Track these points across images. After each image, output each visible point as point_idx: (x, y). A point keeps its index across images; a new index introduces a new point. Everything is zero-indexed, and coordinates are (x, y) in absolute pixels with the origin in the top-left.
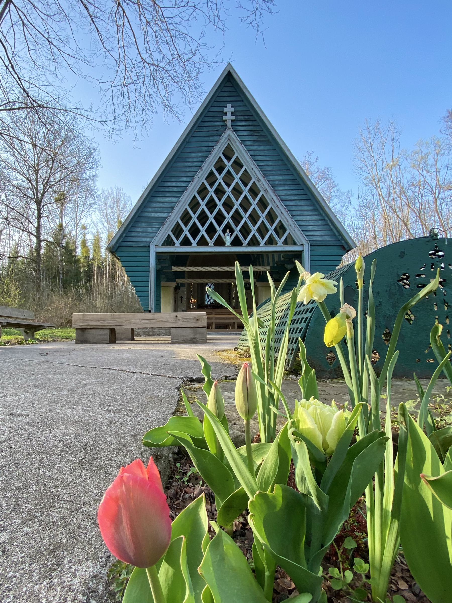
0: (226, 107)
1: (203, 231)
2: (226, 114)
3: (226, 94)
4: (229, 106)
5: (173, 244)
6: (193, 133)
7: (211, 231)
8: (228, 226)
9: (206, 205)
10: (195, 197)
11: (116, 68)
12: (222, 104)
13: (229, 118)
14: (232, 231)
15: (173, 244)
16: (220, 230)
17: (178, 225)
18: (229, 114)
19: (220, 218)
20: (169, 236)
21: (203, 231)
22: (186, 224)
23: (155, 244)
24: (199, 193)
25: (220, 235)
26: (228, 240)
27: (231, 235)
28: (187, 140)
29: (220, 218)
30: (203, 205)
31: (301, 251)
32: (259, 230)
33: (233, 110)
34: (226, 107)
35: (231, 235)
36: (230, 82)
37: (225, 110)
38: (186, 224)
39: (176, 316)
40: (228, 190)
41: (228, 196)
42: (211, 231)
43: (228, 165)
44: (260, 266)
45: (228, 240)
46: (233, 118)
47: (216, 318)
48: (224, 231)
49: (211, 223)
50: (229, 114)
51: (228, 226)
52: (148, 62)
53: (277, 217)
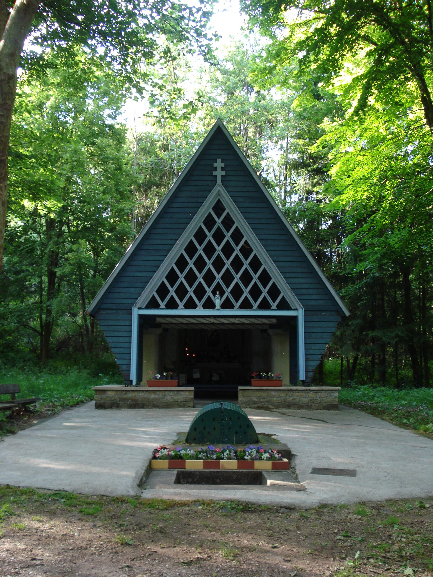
4: (219, 160)
7: (200, 291)
13: (219, 173)
16: (209, 291)
17: (210, 215)
18: (219, 169)
19: (209, 278)
20: (191, 241)
26: (218, 302)
29: (209, 278)
33: (223, 165)
35: (221, 298)
37: (215, 165)
42: (200, 291)
45: (218, 302)
46: (224, 173)
48: (214, 293)
50: (219, 169)
53: (270, 279)
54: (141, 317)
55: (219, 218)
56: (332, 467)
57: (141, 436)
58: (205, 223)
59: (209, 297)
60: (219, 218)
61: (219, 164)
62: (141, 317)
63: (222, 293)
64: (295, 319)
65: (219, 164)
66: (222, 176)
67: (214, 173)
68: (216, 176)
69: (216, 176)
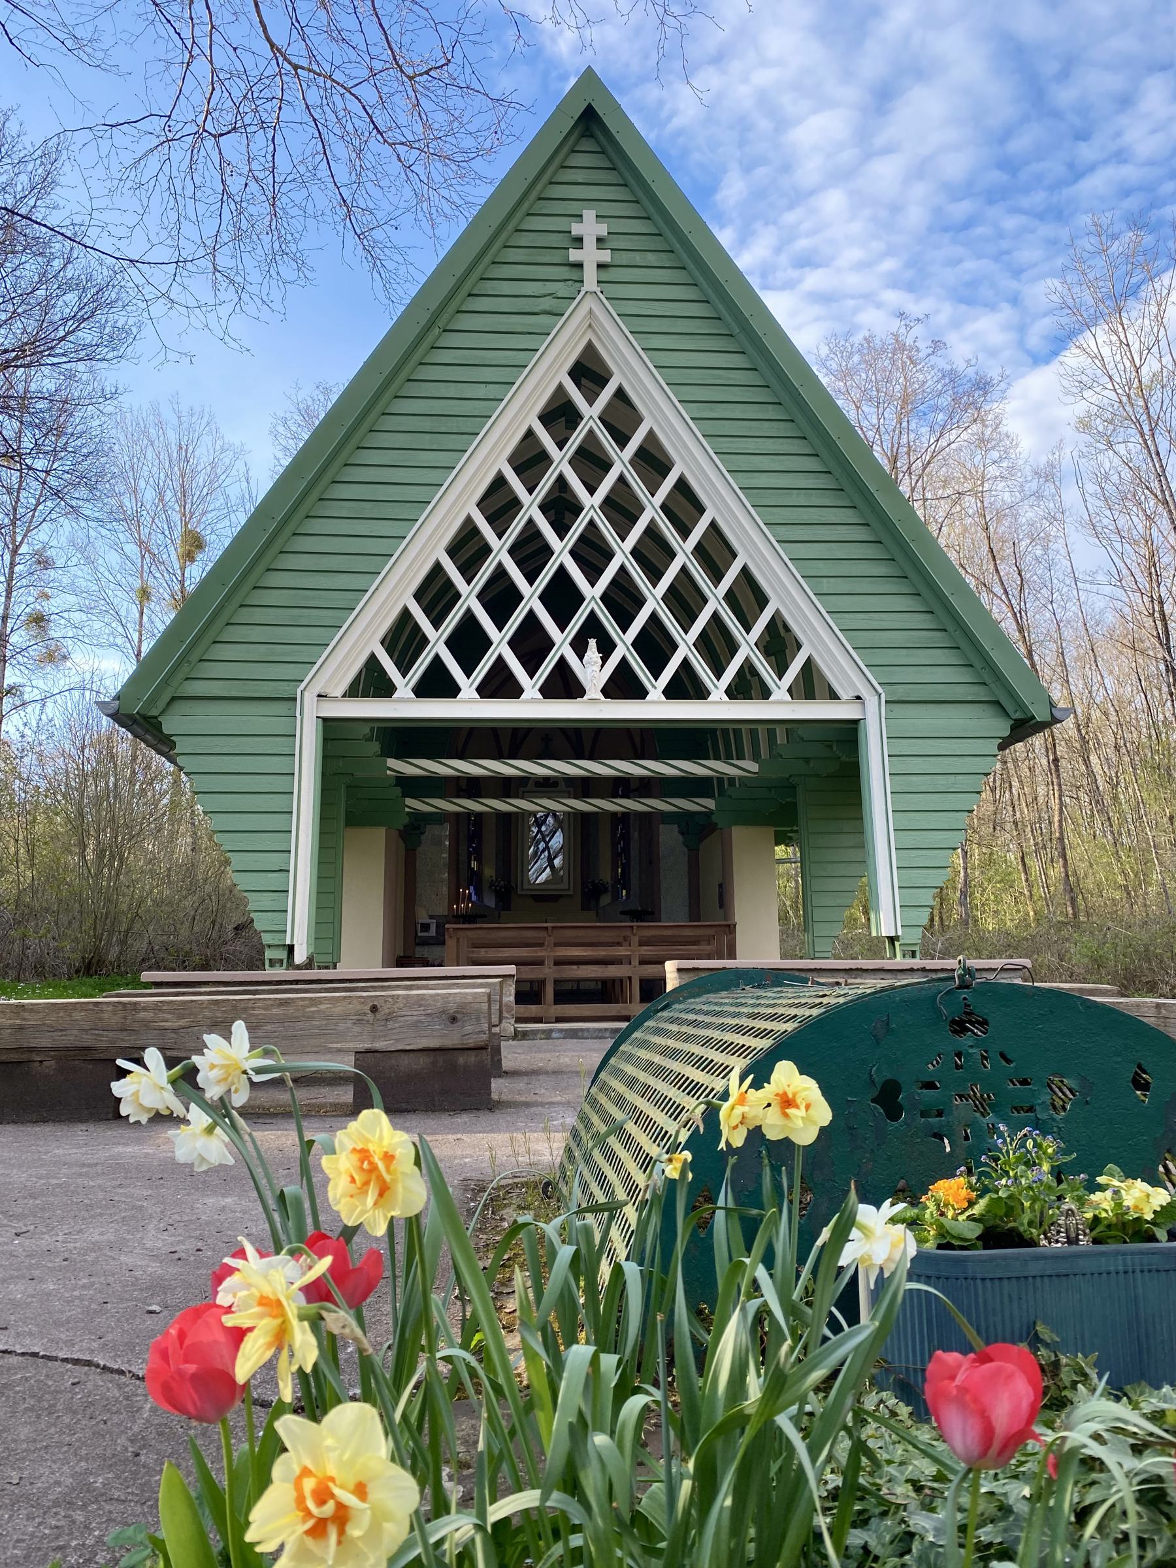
0: (579, 217)
1: (500, 642)
2: (578, 241)
3: (579, 176)
4: (589, 215)
5: (386, 689)
6: (486, 269)
8: (592, 626)
9: (511, 552)
10: (530, 433)
11: (177, 71)
12: (572, 207)
14: (607, 647)
15: (386, 689)
16: (561, 641)
17: (500, 482)
18: (590, 243)
20: (406, 614)
21: (500, 642)
22: (468, 573)
23: (317, 688)
24: (390, 642)
25: (562, 661)
27: (604, 660)
28: (441, 323)
30: (531, 507)
31: (856, 722)
32: (704, 643)
33: (602, 230)
34: (579, 217)
35: (604, 660)
36: (592, 136)
37: (576, 229)
38: (468, 573)
39: (374, 1009)
40: (591, 503)
41: (592, 523)
43: (591, 412)
44: (717, 758)
46: (605, 256)
47: (558, 962)
48: (579, 647)
49: (562, 571)
50: (590, 243)
51: (592, 626)
52: (294, 60)
54: (330, 725)
55: (591, 402)
56: (395, 1549)
57: (483, 990)
58: (452, 551)
59: (562, 660)
60: (591, 402)
61: (590, 227)
62: (330, 725)
63: (607, 647)
64: (849, 732)
65: (590, 227)
66: (601, 266)
67: (574, 255)
68: (579, 266)
69: (579, 266)
